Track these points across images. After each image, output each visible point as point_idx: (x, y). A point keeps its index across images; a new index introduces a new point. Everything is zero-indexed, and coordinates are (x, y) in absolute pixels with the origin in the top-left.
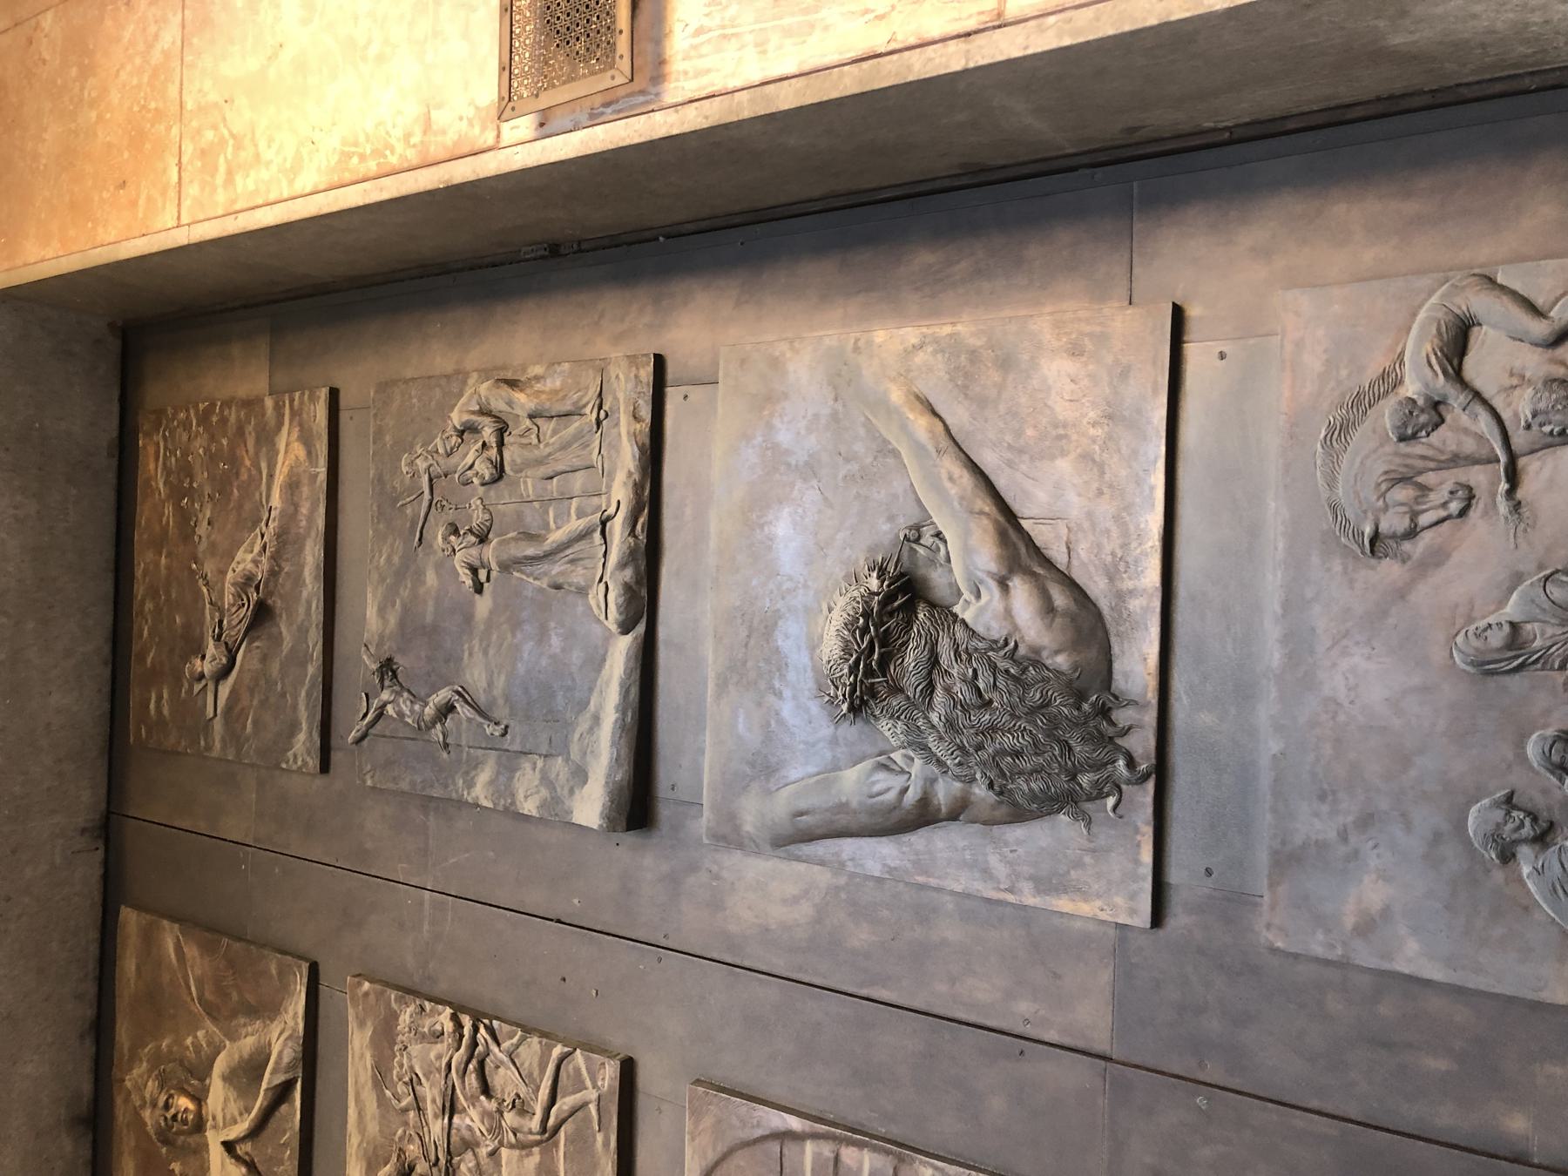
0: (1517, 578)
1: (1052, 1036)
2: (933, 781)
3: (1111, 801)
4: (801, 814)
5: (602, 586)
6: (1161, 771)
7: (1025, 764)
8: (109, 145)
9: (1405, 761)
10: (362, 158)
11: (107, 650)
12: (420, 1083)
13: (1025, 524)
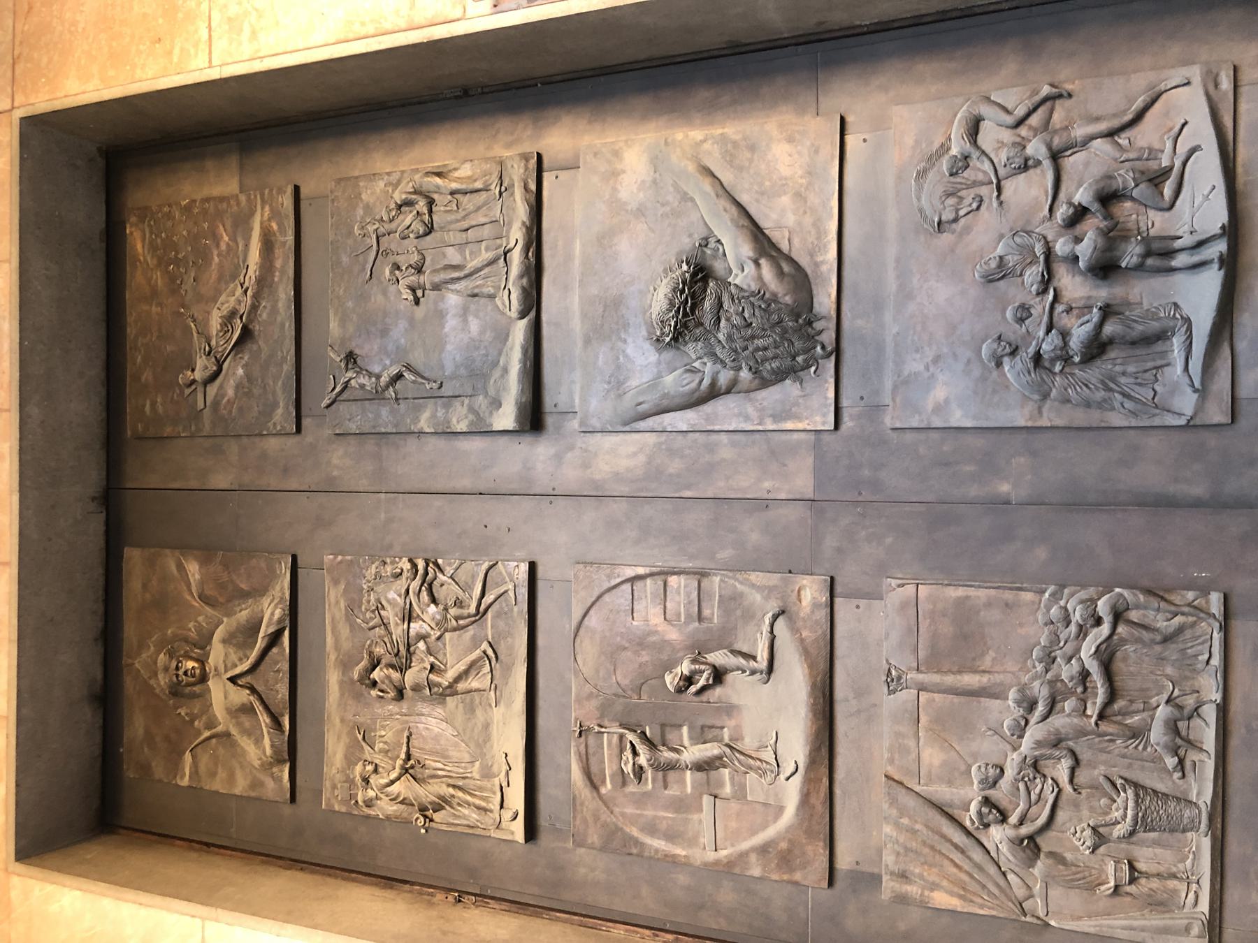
0: (1002, 236)
1: (783, 496)
2: (718, 373)
3: (813, 369)
4: (640, 404)
5: (506, 291)
6: (838, 351)
7: (769, 354)
8: (145, 15)
9: (954, 328)
10: (363, 24)
11: (103, 375)
12: (383, 608)
13: (766, 232)
